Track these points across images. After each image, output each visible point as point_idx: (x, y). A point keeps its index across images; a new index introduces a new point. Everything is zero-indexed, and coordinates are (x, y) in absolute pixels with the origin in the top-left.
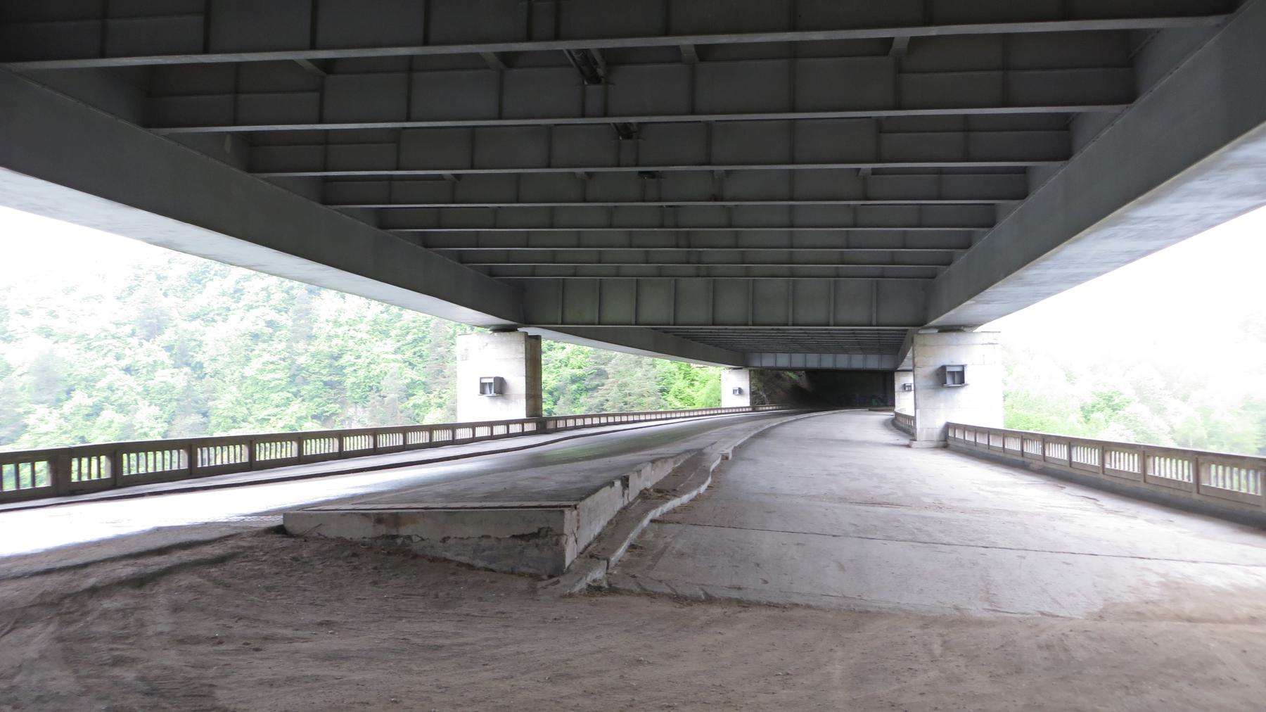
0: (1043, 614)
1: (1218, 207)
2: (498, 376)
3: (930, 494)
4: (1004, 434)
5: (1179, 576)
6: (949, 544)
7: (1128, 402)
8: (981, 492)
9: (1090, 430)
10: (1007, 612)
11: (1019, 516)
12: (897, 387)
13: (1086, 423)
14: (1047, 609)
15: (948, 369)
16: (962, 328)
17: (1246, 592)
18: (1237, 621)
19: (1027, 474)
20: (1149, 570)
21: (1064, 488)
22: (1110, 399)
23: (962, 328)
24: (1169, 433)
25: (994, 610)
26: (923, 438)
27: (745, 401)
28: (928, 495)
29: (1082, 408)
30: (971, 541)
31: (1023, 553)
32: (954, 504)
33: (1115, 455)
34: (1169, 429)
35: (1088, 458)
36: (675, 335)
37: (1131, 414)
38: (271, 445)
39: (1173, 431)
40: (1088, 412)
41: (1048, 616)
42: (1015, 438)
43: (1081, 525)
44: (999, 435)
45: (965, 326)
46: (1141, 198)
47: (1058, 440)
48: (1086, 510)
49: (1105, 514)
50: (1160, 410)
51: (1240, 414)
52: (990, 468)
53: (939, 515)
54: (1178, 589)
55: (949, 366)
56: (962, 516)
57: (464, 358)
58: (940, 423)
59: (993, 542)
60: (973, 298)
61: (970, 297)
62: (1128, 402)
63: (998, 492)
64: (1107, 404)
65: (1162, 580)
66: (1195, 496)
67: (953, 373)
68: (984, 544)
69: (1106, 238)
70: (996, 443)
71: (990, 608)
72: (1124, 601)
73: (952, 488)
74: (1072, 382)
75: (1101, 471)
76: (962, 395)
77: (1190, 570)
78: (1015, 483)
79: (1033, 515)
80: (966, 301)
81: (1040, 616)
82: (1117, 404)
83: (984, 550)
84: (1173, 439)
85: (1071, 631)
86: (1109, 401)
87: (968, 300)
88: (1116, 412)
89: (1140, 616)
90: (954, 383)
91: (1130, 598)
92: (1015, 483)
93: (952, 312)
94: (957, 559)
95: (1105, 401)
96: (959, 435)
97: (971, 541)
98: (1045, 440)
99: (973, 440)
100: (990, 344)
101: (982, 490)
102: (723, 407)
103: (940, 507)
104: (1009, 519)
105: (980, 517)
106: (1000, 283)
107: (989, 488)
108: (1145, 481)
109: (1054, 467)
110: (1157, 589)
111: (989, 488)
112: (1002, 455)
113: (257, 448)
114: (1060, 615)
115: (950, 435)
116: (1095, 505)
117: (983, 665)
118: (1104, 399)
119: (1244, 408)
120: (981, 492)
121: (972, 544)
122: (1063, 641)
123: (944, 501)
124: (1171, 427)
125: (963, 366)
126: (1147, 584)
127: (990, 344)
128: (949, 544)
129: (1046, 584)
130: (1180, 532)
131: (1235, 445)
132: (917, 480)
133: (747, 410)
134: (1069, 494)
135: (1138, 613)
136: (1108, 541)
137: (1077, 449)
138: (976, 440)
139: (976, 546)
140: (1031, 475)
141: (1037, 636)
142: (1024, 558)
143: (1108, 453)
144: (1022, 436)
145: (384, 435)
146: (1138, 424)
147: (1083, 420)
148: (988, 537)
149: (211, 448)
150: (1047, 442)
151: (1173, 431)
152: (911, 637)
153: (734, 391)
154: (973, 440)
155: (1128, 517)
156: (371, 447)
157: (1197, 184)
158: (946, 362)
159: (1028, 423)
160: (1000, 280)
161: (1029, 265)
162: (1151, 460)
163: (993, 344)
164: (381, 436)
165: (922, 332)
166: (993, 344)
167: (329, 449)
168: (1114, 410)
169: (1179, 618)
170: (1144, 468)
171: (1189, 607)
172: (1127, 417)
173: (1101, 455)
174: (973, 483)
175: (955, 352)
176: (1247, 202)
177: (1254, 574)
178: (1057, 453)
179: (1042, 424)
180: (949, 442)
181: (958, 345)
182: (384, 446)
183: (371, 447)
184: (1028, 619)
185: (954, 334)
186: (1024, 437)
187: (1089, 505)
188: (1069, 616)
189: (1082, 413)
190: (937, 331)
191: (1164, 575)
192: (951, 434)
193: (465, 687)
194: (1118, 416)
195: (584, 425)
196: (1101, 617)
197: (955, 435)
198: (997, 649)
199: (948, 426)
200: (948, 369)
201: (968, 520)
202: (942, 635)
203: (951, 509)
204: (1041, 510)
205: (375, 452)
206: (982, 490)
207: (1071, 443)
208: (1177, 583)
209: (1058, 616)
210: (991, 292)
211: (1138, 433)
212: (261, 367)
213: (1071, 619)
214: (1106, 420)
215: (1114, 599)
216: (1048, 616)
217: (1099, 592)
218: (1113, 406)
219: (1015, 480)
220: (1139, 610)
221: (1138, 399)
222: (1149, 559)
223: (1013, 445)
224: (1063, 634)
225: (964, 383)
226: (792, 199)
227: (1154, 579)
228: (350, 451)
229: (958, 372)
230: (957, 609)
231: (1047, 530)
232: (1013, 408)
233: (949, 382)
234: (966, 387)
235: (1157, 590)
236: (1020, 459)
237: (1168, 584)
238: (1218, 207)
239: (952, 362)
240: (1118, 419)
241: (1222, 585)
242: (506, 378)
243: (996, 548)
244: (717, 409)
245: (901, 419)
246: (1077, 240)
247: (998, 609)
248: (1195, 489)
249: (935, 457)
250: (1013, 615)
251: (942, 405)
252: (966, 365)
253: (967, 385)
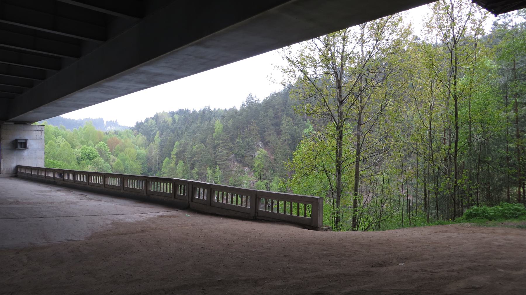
0: (68, 240)
1: (134, 86)
2: (184, 107)
3: (12, 198)
4: (45, 170)
5: (118, 220)
6: (24, 218)
7: (95, 157)
8: (36, 195)
9: (80, 168)
10: (53, 242)
11: (55, 204)
13: (79, 165)
14: (70, 238)
15: (19, 141)
16: (26, 123)
17: (139, 223)
18: (137, 232)
19: (56, 187)
20: (107, 219)
21: (72, 191)
22: (88, 155)
23: (26, 123)
24: (111, 169)
25: (48, 242)
26: (5, 173)
28: (11, 198)
29: (77, 159)
30: (34, 216)
31: (58, 218)
32: (24, 201)
33: (95, 177)
34: (111, 167)
35: (83, 179)
37: (97, 161)
39: (112, 168)
40: (80, 161)
41: (71, 241)
42: (51, 172)
43: (81, 205)
44: (43, 170)
45: (28, 122)
46: (108, 79)
47: (70, 172)
48: (82, 199)
49: (90, 200)
50: (107, 160)
51: (135, 161)
52: (39, 185)
53: (17, 206)
54: (118, 224)
55: (19, 139)
56: (29, 206)
58: (14, 165)
59: (45, 215)
60: (33, 110)
61: (31, 109)
62: (95, 157)
63: (44, 195)
64: (87, 157)
65: (112, 222)
66: (122, 191)
67: (21, 143)
68: (41, 216)
69: (94, 92)
70: (42, 174)
71: (46, 241)
72: (99, 231)
73: (22, 194)
74: (73, 148)
75: (88, 184)
76: (26, 153)
77: (121, 217)
78: (51, 191)
79: (61, 203)
80: (29, 111)
81: (67, 241)
82: (91, 157)
83: (41, 219)
84: (112, 171)
85: (81, 244)
86: (88, 156)
87: (30, 110)
88: (91, 160)
89: (105, 235)
90: (21, 147)
91: (101, 230)
92: (51, 191)
93: (22, 115)
94: (29, 223)
95: (86, 156)
96: (23, 171)
97: (34, 216)
98: (64, 172)
99: (30, 173)
100: (39, 130)
101: (37, 194)
103: (17, 202)
104: (50, 205)
105: (37, 205)
106: (46, 105)
107: (39, 193)
108: (104, 187)
109: (68, 183)
110: (111, 225)
111: (39, 193)
112: (44, 179)
114: (75, 240)
115: (18, 171)
116: (85, 197)
117: (47, 263)
118: (86, 155)
119: (137, 159)
120: (36, 195)
121: (35, 217)
122: (78, 248)
123: (19, 200)
124: (112, 166)
125: (26, 140)
126: (107, 224)
127: (39, 130)
128: (24, 218)
129: (69, 229)
130: (117, 205)
131: (133, 173)
132: (4, 191)
134: (74, 194)
135: (104, 234)
136: (92, 210)
137: (78, 175)
138: (31, 173)
139: (37, 218)
140: (58, 187)
141: (68, 249)
142: (59, 220)
143: (91, 177)
144: (54, 171)
146: (99, 165)
147: (77, 164)
148: (42, 213)
150: (65, 173)
151: (112, 168)
152: (12, 258)
154: (30, 173)
155: (98, 201)
157: (127, 77)
158: (18, 137)
159: (54, 165)
160: (47, 103)
161: (60, 98)
163: (41, 131)
165: (5, 123)
166: (41, 131)
168: (90, 160)
169: (119, 234)
171: (122, 230)
172: (95, 163)
174: (32, 192)
175: (21, 135)
176: (144, 86)
177: (142, 216)
178: (69, 177)
179: (60, 165)
180: (18, 174)
181: (24, 130)
184: (63, 243)
185: (22, 125)
186: (55, 171)
187: (83, 197)
188: (78, 239)
189: (77, 161)
190: (13, 123)
191: (112, 220)
192: (19, 170)
193: (475, 79)
194: (92, 162)
196: (91, 238)
197: (21, 171)
198: (52, 256)
199: (18, 167)
200: (19, 141)
201: (32, 207)
202: (26, 255)
203: (23, 203)
204: (64, 201)
206: (37, 194)
207: (75, 173)
208: (117, 222)
209: (75, 240)
210: (42, 108)
211: (99, 169)
213: (80, 241)
214: (87, 164)
215: (95, 231)
216: (71, 241)
217: (89, 229)
218: (90, 158)
219: (51, 189)
220: (105, 233)
221: (100, 155)
222: (107, 215)
223: (50, 175)
224: (78, 246)
225: (26, 147)
227: (109, 222)
229: (23, 142)
230: (31, 244)
231: (67, 208)
232: (47, 159)
233: (19, 147)
234: (27, 149)
235: (111, 226)
236: (53, 180)
237: (114, 223)
238: (134, 86)
239: (21, 138)
240: (92, 163)
241: (132, 221)
243: (46, 217)
246: (82, 91)
247: (50, 241)
248: (122, 189)
249: (11, 181)
250: (56, 243)
251: (15, 157)
252: (28, 139)
253: (27, 148)
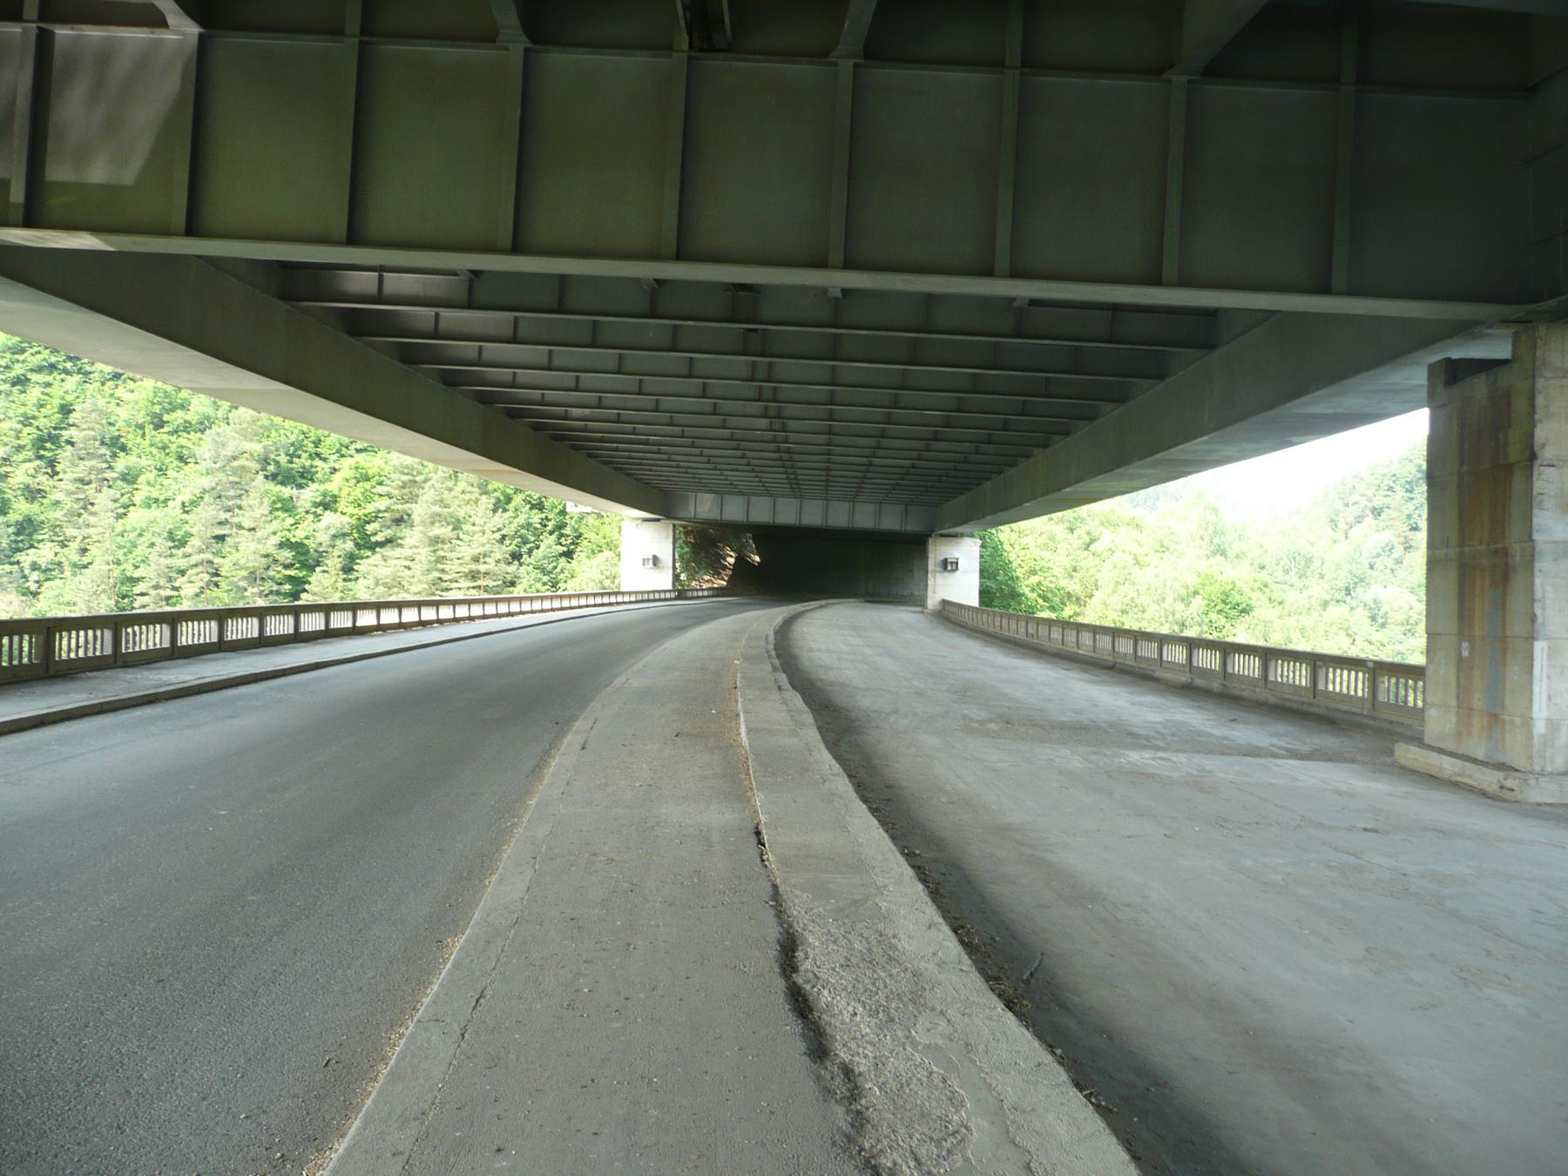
12: (933, 562)
27: (662, 580)
36: (636, 479)
38: (141, 629)
57: (986, 574)
67: (952, 563)
102: (622, 590)
113: (57, 637)
125: (957, 559)
133: (668, 595)
143: (1197, 650)
145: (207, 622)
149: (64, 633)
153: (644, 560)
156: (166, 644)
162: (1273, 662)
164: (184, 623)
167: (199, 639)
170: (1224, 664)
173: (1188, 651)
182: (282, 633)
183: (166, 644)
195: (455, 617)
205: (353, 632)
212: (404, 531)
226: (831, 405)
228: (276, 636)
242: (658, 556)
244: (616, 594)
245: (947, 606)
